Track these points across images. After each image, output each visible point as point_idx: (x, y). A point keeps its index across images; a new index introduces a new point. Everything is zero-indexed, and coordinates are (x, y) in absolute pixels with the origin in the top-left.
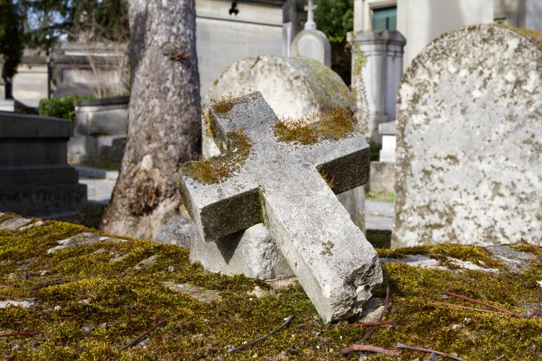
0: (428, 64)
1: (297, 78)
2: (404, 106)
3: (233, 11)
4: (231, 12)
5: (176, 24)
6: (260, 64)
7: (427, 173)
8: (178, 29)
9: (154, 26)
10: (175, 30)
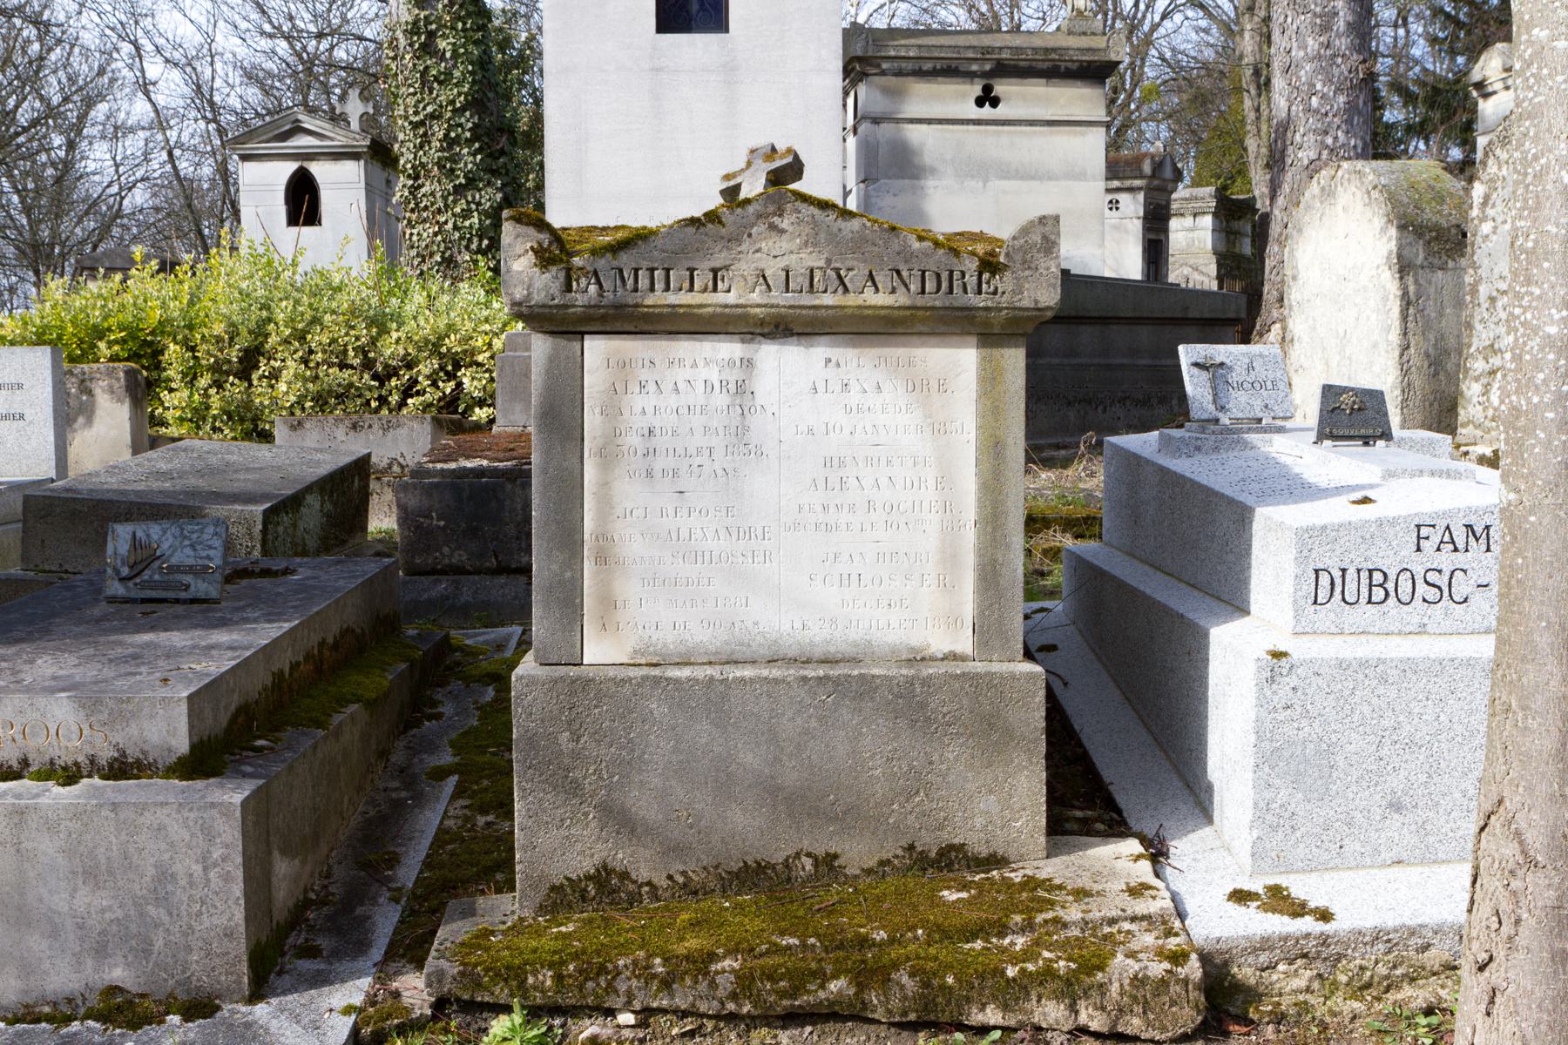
0: (1498, 152)
1: (1375, 187)
2: (1475, 212)
3: (987, 98)
4: (980, 102)
5: (1332, 133)
6: (1340, 173)
7: (1492, 299)
8: (1336, 138)
9: (1298, 137)
10: (1329, 141)
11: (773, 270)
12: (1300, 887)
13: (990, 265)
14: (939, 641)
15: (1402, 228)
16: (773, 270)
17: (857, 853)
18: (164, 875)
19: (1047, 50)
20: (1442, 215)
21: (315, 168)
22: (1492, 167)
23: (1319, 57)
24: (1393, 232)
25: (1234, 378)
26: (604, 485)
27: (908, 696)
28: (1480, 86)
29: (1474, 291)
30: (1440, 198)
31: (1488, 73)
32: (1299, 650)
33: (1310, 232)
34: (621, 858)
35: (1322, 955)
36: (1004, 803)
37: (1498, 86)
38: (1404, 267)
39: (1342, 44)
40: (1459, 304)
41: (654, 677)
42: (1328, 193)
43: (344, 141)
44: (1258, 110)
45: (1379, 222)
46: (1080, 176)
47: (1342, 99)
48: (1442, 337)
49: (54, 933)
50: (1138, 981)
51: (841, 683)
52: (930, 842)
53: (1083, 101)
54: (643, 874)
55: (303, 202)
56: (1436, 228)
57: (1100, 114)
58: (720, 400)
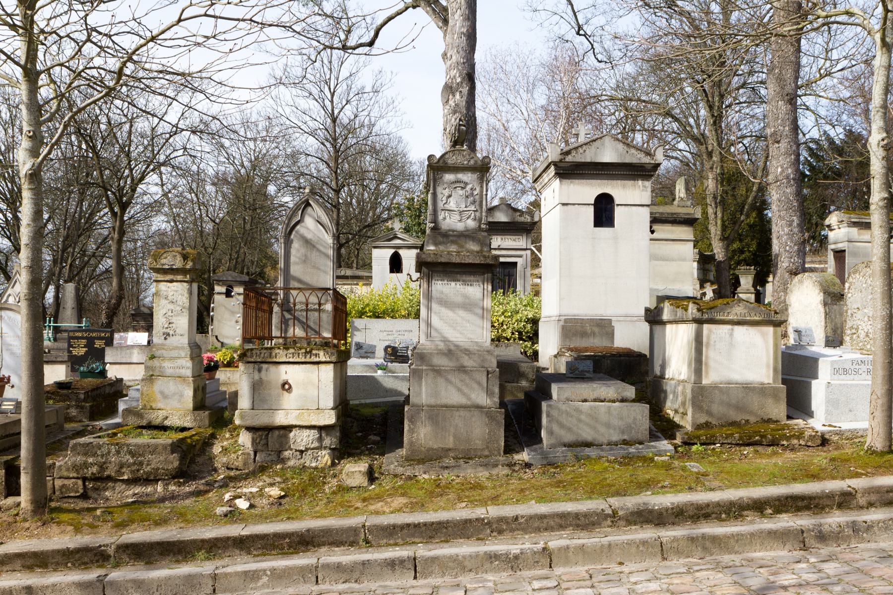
11: (738, 313)
12: (834, 424)
13: (776, 313)
14: (766, 381)
15: (824, 293)
16: (738, 313)
17: (753, 419)
18: (635, 419)
19: (672, 214)
20: (836, 289)
21: (401, 252)
22: (851, 279)
23: (789, 234)
24: (822, 294)
25: (803, 333)
26: (707, 351)
27: (762, 390)
28: (829, 226)
29: (847, 312)
30: (834, 285)
31: (832, 222)
32: (832, 382)
33: (794, 292)
34: (710, 420)
35: (840, 433)
36: (778, 410)
37: (836, 227)
38: (825, 304)
39: (796, 230)
40: (841, 315)
41: (714, 387)
42: (801, 282)
43: (413, 242)
44: (716, 214)
45: (817, 291)
46: (684, 260)
47: (796, 247)
48: (836, 324)
49: (615, 429)
50: (810, 436)
51: (748, 388)
52: (766, 418)
53: (686, 232)
54: (714, 423)
55: (396, 264)
56: (834, 293)
57: (692, 237)
58: (728, 336)
